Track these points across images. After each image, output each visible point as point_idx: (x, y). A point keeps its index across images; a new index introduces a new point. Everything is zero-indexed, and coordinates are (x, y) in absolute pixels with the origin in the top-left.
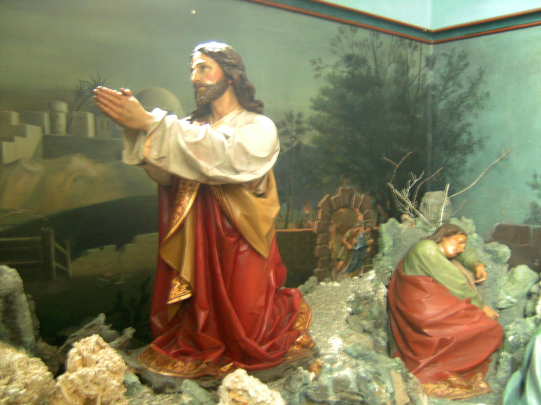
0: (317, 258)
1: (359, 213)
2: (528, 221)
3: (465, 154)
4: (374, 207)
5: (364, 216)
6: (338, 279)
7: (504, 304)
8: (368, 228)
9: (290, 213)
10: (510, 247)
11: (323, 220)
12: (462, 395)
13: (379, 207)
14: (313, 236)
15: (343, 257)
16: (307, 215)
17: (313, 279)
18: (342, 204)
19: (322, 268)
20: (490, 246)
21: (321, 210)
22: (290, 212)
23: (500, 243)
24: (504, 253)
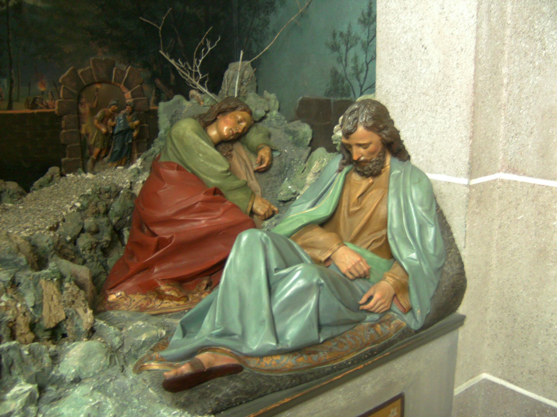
0: (64, 145)
1: (125, 90)
2: (328, 93)
3: (268, 13)
4: (151, 81)
5: (132, 93)
6: (96, 170)
7: (283, 196)
8: (128, 107)
9: (14, 90)
10: (312, 127)
11: (65, 99)
12: (170, 307)
13: (158, 82)
14: (55, 119)
15: (98, 143)
16: (43, 93)
17: (53, 170)
18: (95, 78)
19: (70, 156)
20: (291, 126)
21: (62, 86)
22: (14, 89)
23: (303, 122)
24: (305, 133)
